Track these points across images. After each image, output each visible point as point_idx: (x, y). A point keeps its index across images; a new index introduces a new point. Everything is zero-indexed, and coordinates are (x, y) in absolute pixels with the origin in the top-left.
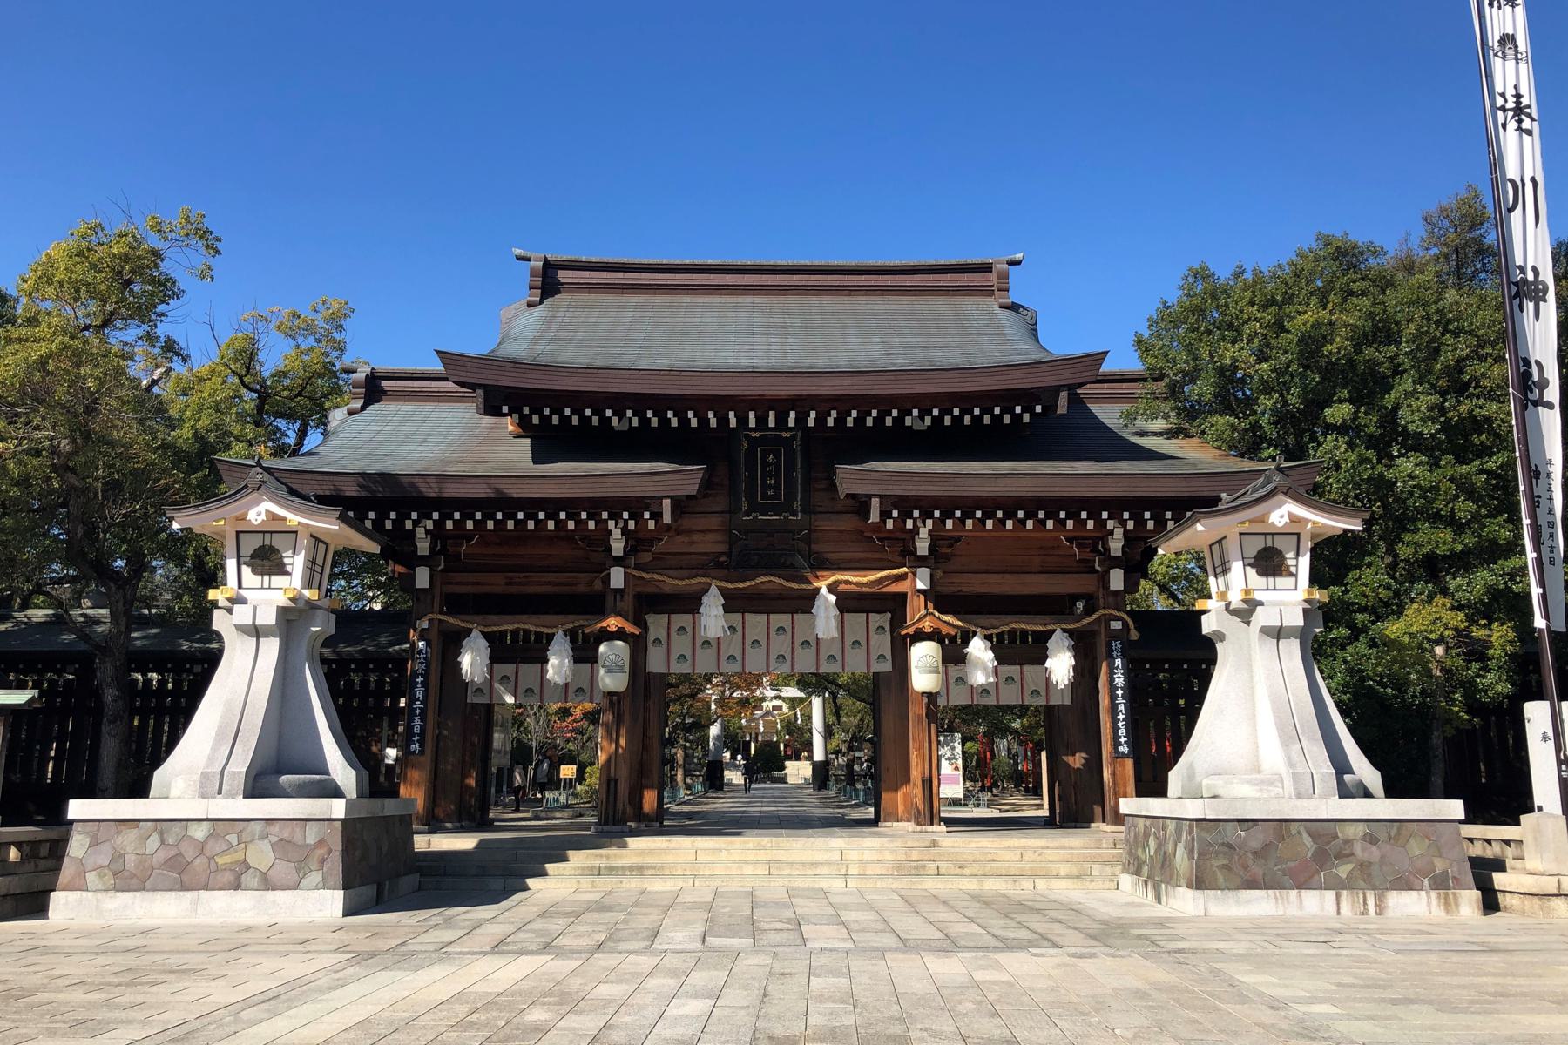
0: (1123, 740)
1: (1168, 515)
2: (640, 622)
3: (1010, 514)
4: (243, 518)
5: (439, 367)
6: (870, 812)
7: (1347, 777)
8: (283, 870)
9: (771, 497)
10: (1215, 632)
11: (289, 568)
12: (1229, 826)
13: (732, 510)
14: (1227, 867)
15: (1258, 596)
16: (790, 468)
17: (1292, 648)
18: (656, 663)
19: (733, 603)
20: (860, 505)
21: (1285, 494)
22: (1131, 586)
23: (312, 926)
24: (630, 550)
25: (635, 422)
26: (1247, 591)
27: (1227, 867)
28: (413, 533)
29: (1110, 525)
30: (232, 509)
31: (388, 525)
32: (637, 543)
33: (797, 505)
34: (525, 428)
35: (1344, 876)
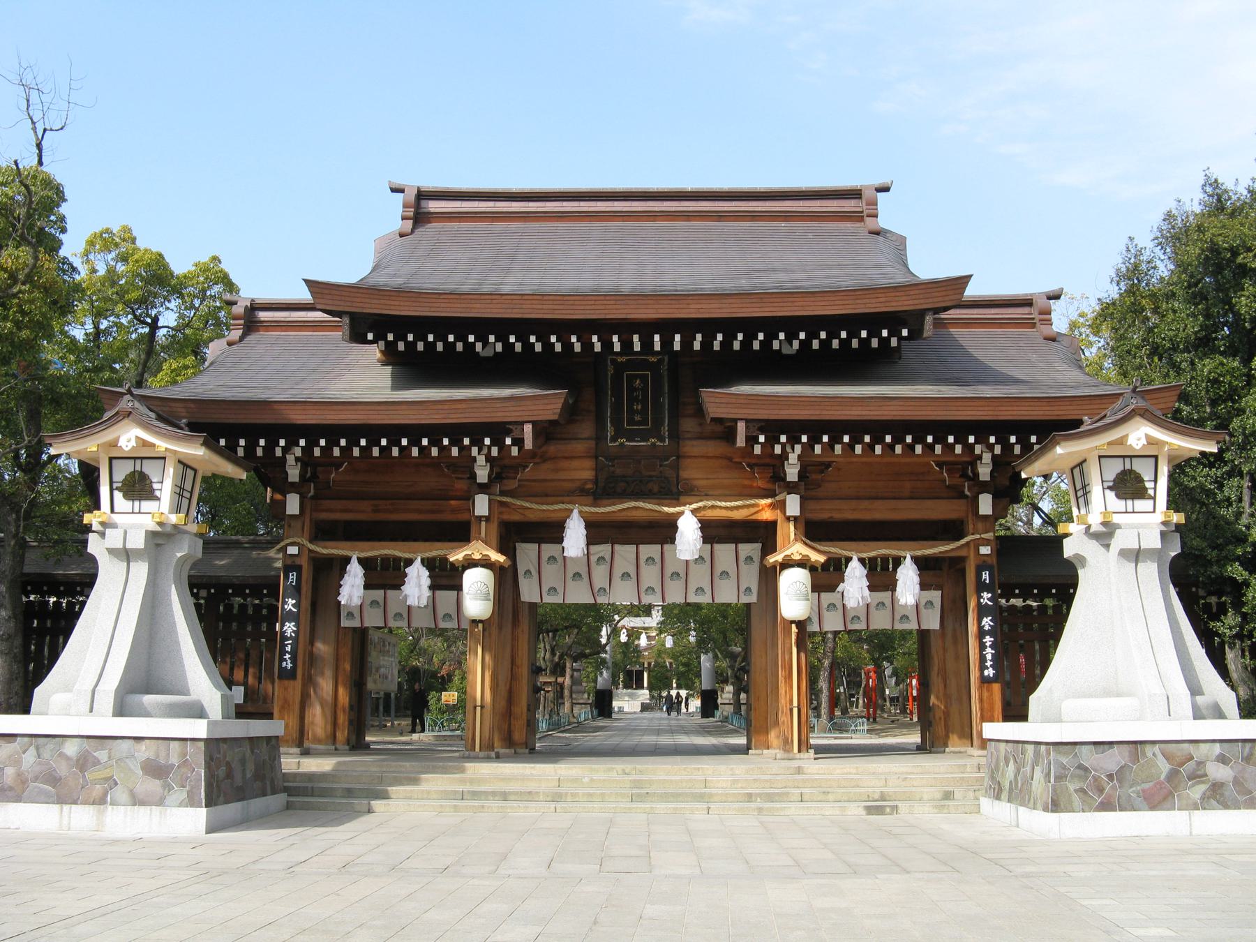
0: (989, 664)
1: (1033, 439)
2: (505, 547)
3: (920, 439)
4: (114, 444)
5: (305, 295)
6: (742, 741)
7: (1198, 698)
10: (1077, 556)
11: (157, 493)
12: (1085, 749)
13: (600, 437)
14: (1082, 790)
15: (1116, 519)
16: (657, 392)
17: (1151, 573)
18: (529, 592)
19: (597, 532)
20: (726, 431)
21: (1142, 416)
22: (1000, 511)
23: (175, 841)
24: (495, 477)
25: (499, 347)
26: (1106, 513)
27: (1082, 790)
29: (978, 449)
30: (107, 436)
31: (259, 452)
32: (501, 469)
34: (391, 357)
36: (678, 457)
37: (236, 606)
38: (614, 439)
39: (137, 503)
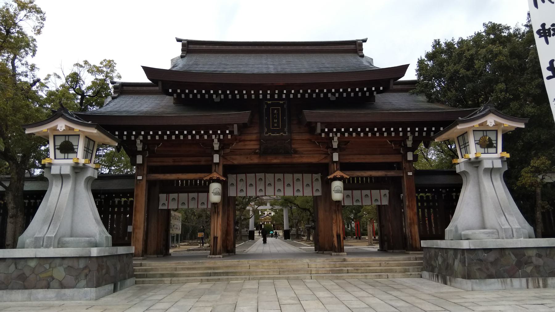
5: (144, 79)
8: (70, 279)
9: (276, 127)
14: (479, 269)
18: (232, 193)
24: (222, 148)
27: (479, 269)
28: (135, 142)
32: (224, 144)
33: (286, 129)
35: (529, 271)
36: (291, 140)
37: (117, 202)
38: (267, 133)
39: (66, 155)
